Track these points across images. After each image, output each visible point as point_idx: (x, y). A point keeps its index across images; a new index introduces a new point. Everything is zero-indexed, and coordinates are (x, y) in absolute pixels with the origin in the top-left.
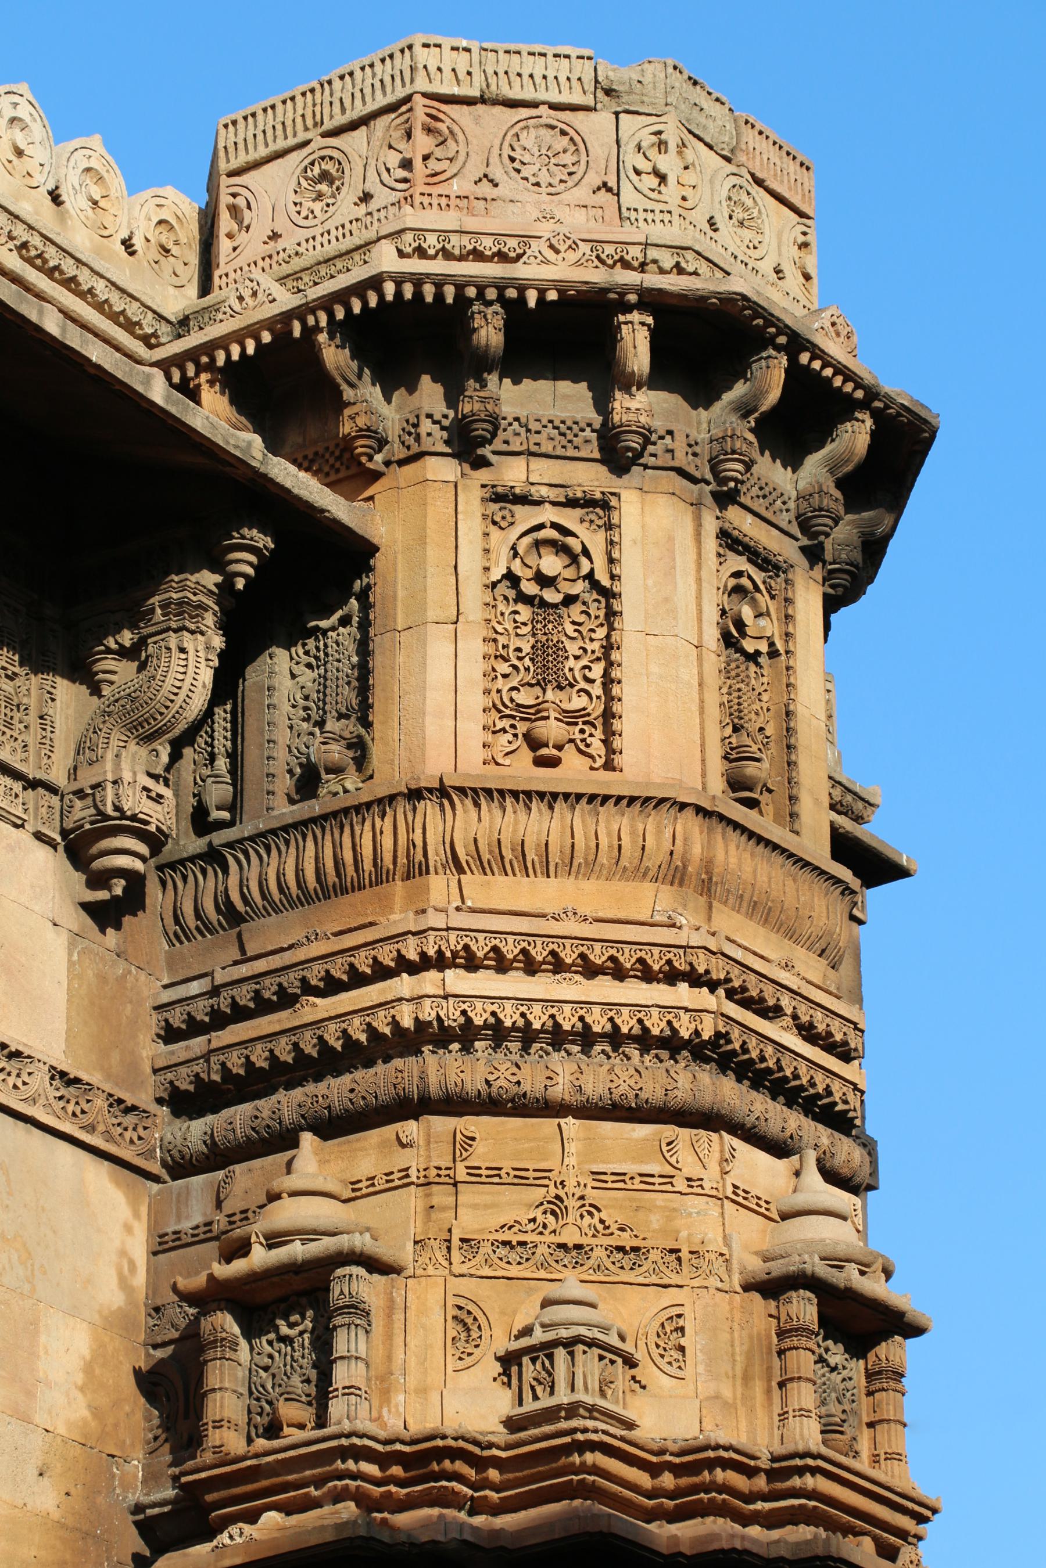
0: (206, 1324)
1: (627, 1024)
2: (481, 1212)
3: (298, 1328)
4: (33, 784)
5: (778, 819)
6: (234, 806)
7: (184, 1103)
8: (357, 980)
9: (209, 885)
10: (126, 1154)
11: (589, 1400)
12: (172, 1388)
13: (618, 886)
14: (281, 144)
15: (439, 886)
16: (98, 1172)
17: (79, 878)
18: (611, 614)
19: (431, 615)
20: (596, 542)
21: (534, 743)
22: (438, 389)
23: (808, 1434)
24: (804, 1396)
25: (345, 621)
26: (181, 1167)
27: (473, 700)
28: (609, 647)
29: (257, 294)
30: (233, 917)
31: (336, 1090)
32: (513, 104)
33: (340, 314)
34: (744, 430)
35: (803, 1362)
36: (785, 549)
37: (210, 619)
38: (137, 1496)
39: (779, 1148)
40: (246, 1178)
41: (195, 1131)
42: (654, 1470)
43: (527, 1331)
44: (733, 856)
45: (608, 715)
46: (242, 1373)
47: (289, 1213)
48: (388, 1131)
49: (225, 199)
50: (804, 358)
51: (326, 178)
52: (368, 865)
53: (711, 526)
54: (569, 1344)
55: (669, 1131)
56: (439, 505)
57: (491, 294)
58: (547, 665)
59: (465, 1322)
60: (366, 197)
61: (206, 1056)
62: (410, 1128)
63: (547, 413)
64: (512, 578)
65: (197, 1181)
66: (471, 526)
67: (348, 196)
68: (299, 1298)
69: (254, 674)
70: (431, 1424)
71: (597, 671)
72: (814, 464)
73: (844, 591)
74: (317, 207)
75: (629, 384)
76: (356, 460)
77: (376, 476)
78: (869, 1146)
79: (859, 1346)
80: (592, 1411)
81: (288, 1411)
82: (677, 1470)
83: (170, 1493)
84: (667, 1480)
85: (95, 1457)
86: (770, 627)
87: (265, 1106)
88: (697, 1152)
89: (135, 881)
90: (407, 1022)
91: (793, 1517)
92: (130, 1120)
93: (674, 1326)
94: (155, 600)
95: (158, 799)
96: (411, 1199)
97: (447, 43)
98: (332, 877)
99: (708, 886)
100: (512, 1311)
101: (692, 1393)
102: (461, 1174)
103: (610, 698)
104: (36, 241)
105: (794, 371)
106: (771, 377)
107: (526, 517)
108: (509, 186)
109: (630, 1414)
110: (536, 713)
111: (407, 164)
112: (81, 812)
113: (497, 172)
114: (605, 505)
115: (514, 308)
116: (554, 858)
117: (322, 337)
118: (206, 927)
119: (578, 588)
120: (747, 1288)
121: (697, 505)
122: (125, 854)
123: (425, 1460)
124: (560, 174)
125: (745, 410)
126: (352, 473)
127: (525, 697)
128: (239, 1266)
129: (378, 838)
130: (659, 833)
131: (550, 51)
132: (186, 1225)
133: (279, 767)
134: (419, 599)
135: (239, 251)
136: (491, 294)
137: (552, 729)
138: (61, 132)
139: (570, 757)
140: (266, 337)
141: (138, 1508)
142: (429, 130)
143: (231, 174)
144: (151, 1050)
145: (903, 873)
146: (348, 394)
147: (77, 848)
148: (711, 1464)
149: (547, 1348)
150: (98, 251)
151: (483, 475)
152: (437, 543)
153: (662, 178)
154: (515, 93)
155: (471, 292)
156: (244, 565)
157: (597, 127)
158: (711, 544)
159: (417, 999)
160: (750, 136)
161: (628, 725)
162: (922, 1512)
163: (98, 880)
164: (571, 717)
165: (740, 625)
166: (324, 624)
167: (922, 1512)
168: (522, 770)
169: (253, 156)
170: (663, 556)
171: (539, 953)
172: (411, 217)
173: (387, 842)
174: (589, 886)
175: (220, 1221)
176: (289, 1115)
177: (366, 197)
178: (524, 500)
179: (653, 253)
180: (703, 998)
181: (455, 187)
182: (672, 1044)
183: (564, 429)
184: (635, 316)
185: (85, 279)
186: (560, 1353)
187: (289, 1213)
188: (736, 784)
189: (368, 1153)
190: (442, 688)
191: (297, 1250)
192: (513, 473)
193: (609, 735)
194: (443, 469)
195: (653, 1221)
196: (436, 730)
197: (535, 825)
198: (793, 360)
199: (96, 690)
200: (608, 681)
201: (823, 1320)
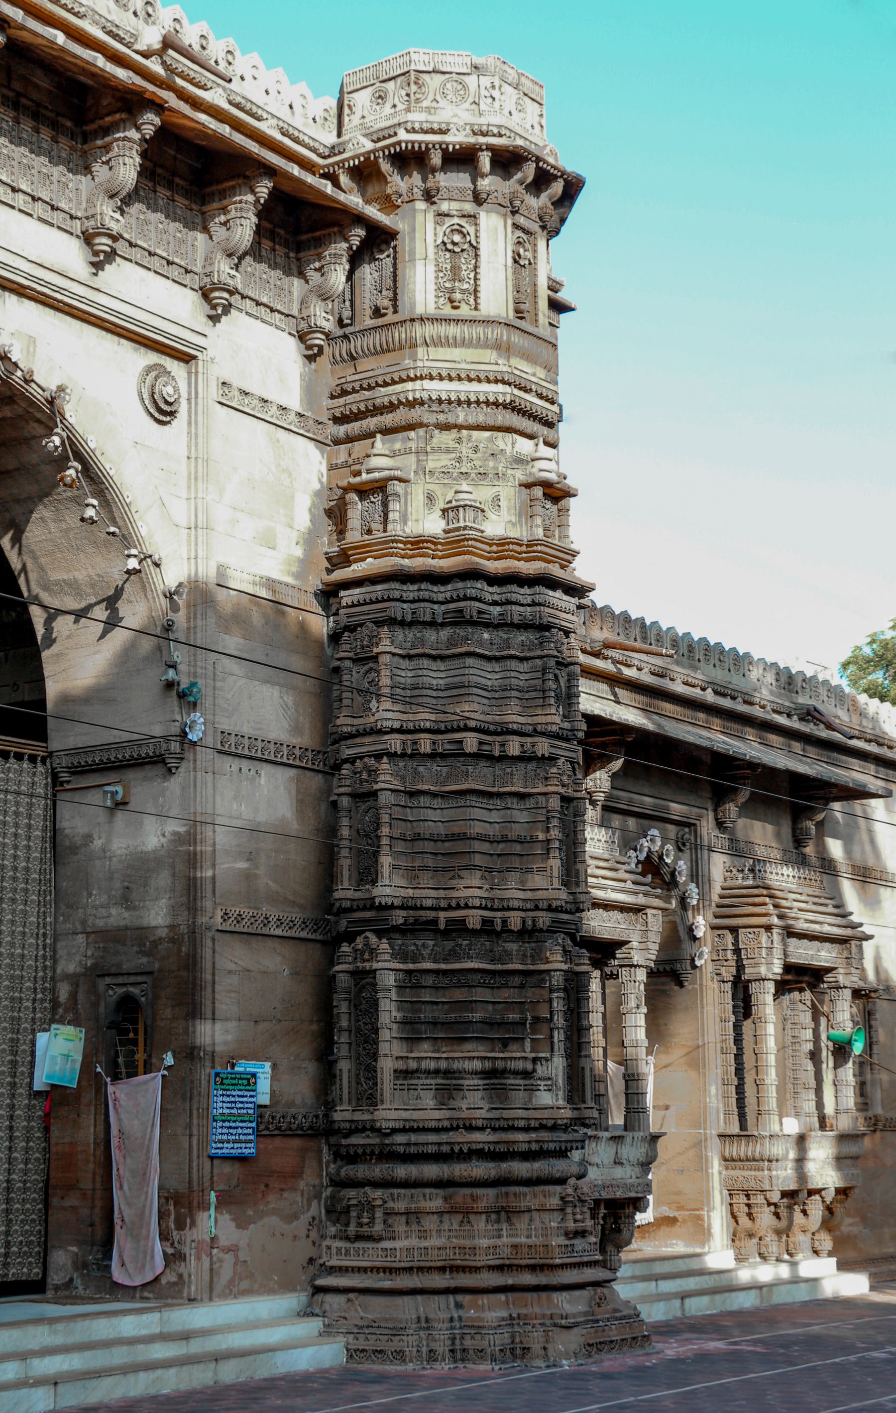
0: (347, 497)
1: (482, 398)
2: (433, 463)
3: (377, 499)
4: (288, 316)
5: (531, 323)
6: (352, 318)
7: (339, 420)
8: (394, 382)
9: (344, 346)
10: (319, 438)
11: (470, 524)
12: (336, 515)
13: (479, 351)
14: (365, 84)
15: (421, 351)
16: (311, 445)
17: (303, 346)
18: (477, 256)
19: (417, 256)
20: (471, 230)
21: (451, 301)
22: (420, 176)
23: (540, 533)
24: (539, 521)
25: (388, 256)
26: (337, 442)
27: (432, 287)
28: (476, 267)
29: (360, 145)
30: (353, 358)
31: (388, 420)
32: (444, 73)
33: (387, 153)
34: (521, 189)
35: (538, 509)
36: (535, 227)
37: (344, 260)
38: (326, 549)
39: (531, 437)
40: (359, 448)
41: (342, 430)
42: (490, 545)
43: (450, 502)
44: (516, 338)
45: (476, 291)
46: (359, 513)
47: (375, 462)
48: (405, 434)
49: (346, 102)
50: (541, 164)
51: (381, 97)
52: (397, 343)
53: (510, 222)
54: (464, 506)
55: (495, 434)
56: (419, 218)
57: (437, 146)
58: (455, 270)
59: (430, 498)
60: (394, 106)
61: (345, 405)
62: (412, 434)
63: (455, 185)
64: (444, 243)
65: (342, 446)
66: (430, 225)
67: (388, 105)
69: (357, 274)
70: (420, 532)
71: (472, 275)
72: (544, 197)
73: (553, 233)
74: (378, 107)
75: (483, 176)
76: (390, 201)
77: (399, 207)
78: (560, 406)
79: (556, 500)
80: (471, 528)
81: (374, 526)
82: (498, 545)
83: (337, 549)
84: (494, 548)
85: (310, 540)
86: (529, 255)
87: (364, 423)
88: (503, 441)
89: (321, 348)
90: (411, 398)
91: (534, 559)
92: (320, 426)
94: (327, 253)
95: (328, 320)
96: (413, 458)
97: (422, 51)
98: (385, 347)
100: (444, 496)
101: (501, 520)
102: (429, 449)
103: (476, 285)
104: (286, 126)
105: (538, 168)
106: (529, 171)
107: (449, 222)
108: (442, 103)
109: (483, 528)
110: (452, 290)
111: (408, 95)
112: (303, 325)
113: (438, 98)
114: (475, 217)
115: (445, 152)
116: (458, 341)
117: (381, 160)
118: (343, 360)
119: (466, 246)
120: (520, 485)
121: (505, 215)
122: (318, 340)
123: (418, 543)
124: (459, 98)
125: (521, 182)
126: (389, 204)
127: (448, 285)
128: (358, 479)
129: (399, 334)
130: (494, 333)
131: (456, 53)
132: (339, 461)
133: (367, 306)
134: (413, 252)
135: (351, 122)
136: (437, 146)
137: (458, 296)
138: (293, 82)
139: (463, 306)
140: (362, 159)
141: (327, 553)
142: (416, 83)
143: (349, 93)
144: (327, 402)
145: (573, 309)
146: (389, 179)
147: (302, 337)
148: (508, 543)
149: (457, 507)
150: (305, 125)
151: (434, 207)
152: (422, 233)
153: (494, 99)
154: (444, 69)
155: (430, 146)
156: (356, 242)
157: (471, 81)
158: (509, 228)
159: (414, 391)
160: (523, 80)
161: (482, 295)
162: (574, 554)
163: (309, 347)
164: (463, 291)
165: (519, 255)
166: (381, 257)
167: (574, 554)
168: (447, 311)
169: (356, 87)
170: (494, 233)
171: (453, 375)
172: (411, 117)
173: (403, 336)
174: (471, 351)
175: (351, 462)
176: (373, 428)
177: (394, 106)
178: (448, 215)
179: (491, 128)
180: (507, 389)
181: (425, 104)
183: (461, 190)
184: (485, 153)
185: (302, 137)
186: (461, 509)
189: (397, 442)
190: (423, 287)
191: (376, 475)
192: (445, 207)
193: (476, 298)
194: (421, 205)
196: (419, 298)
197: (453, 330)
198: (537, 164)
199: (307, 282)
200: (476, 279)
201: (544, 494)
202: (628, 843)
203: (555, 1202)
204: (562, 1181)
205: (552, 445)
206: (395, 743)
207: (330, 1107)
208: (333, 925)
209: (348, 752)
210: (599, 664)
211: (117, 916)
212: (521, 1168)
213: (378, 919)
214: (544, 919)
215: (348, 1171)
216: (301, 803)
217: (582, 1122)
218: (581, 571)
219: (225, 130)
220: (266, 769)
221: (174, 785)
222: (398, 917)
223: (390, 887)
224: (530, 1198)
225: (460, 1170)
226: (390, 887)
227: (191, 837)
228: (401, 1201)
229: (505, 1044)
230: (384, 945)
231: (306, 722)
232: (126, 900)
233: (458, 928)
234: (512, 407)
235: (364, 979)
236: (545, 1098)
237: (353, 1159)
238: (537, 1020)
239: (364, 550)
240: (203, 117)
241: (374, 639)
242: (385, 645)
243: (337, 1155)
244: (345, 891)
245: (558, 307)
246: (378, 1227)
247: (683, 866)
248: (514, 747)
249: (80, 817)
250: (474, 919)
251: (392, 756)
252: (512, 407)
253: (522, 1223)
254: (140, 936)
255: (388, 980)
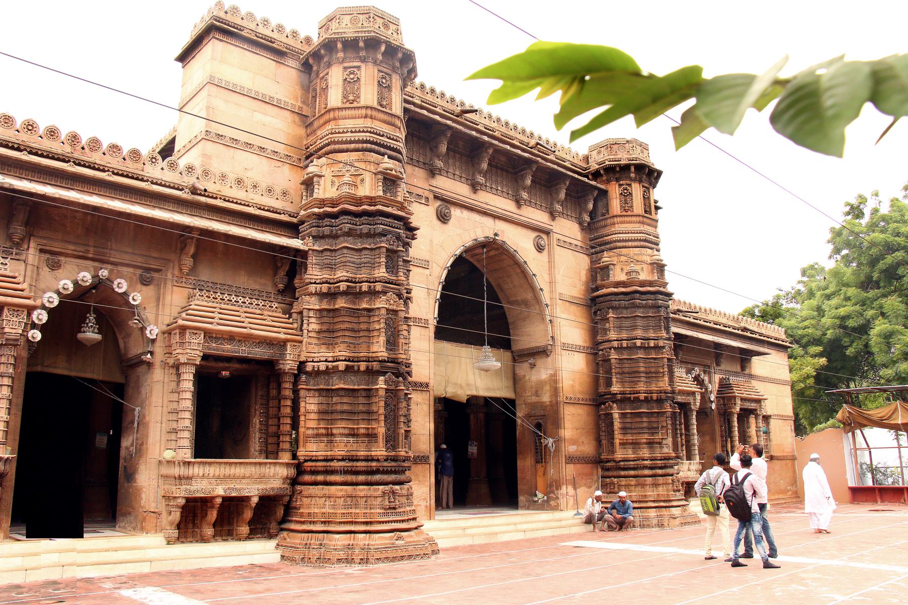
2: (623, 258)
7: (592, 247)
26: (593, 254)
29: (594, 166)
39: (652, 249)
47: (604, 259)
51: (599, 152)
58: (626, 200)
59: (622, 269)
68: (606, 269)
93: (642, 269)
99: (643, 223)
100: (627, 269)
123: (618, 284)
129: (609, 221)
130: (638, 219)
145: (677, 148)
152: (614, 190)
162: (667, 283)
167: (667, 283)
182: (640, 240)
187: (604, 259)
188: (646, 212)
190: (615, 205)
195: (640, 258)
202: (689, 372)
203: (670, 481)
204: (672, 475)
205: (658, 250)
206: (615, 344)
207: (600, 455)
208: (599, 401)
209: (601, 348)
210: (677, 316)
211: (534, 399)
212: (660, 472)
213: (613, 397)
214: (663, 396)
215: (606, 473)
216: (587, 363)
217: (678, 457)
218: (670, 289)
219: (556, 167)
220: (576, 353)
221: (549, 359)
222: (619, 397)
223: (615, 388)
224: (661, 480)
225: (640, 472)
226: (615, 388)
227: (555, 375)
228: (623, 481)
229: (653, 434)
230: (615, 405)
231: (587, 339)
232: (537, 394)
233: (637, 399)
234: (645, 240)
235: (609, 416)
236: (665, 450)
237: (608, 470)
238: (663, 427)
239: (603, 287)
240: (549, 164)
241: (608, 313)
242: (611, 315)
243: (603, 469)
244: (602, 389)
245: (657, 208)
246: (616, 490)
247: (706, 378)
248: (652, 344)
249: (523, 369)
250: (642, 396)
251: (615, 348)
252: (645, 240)
253: (660, 489)
254: (541, 405)
255: (616, 416)
